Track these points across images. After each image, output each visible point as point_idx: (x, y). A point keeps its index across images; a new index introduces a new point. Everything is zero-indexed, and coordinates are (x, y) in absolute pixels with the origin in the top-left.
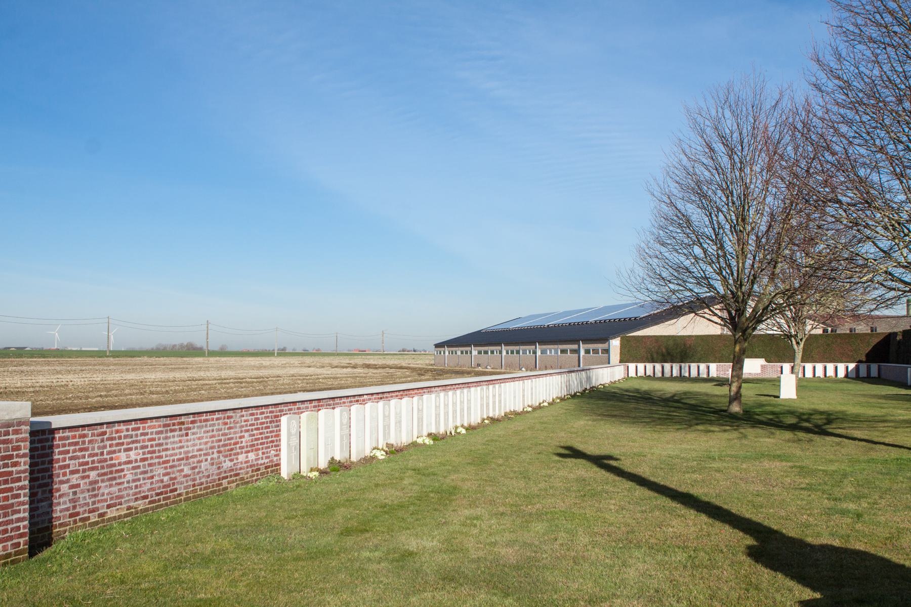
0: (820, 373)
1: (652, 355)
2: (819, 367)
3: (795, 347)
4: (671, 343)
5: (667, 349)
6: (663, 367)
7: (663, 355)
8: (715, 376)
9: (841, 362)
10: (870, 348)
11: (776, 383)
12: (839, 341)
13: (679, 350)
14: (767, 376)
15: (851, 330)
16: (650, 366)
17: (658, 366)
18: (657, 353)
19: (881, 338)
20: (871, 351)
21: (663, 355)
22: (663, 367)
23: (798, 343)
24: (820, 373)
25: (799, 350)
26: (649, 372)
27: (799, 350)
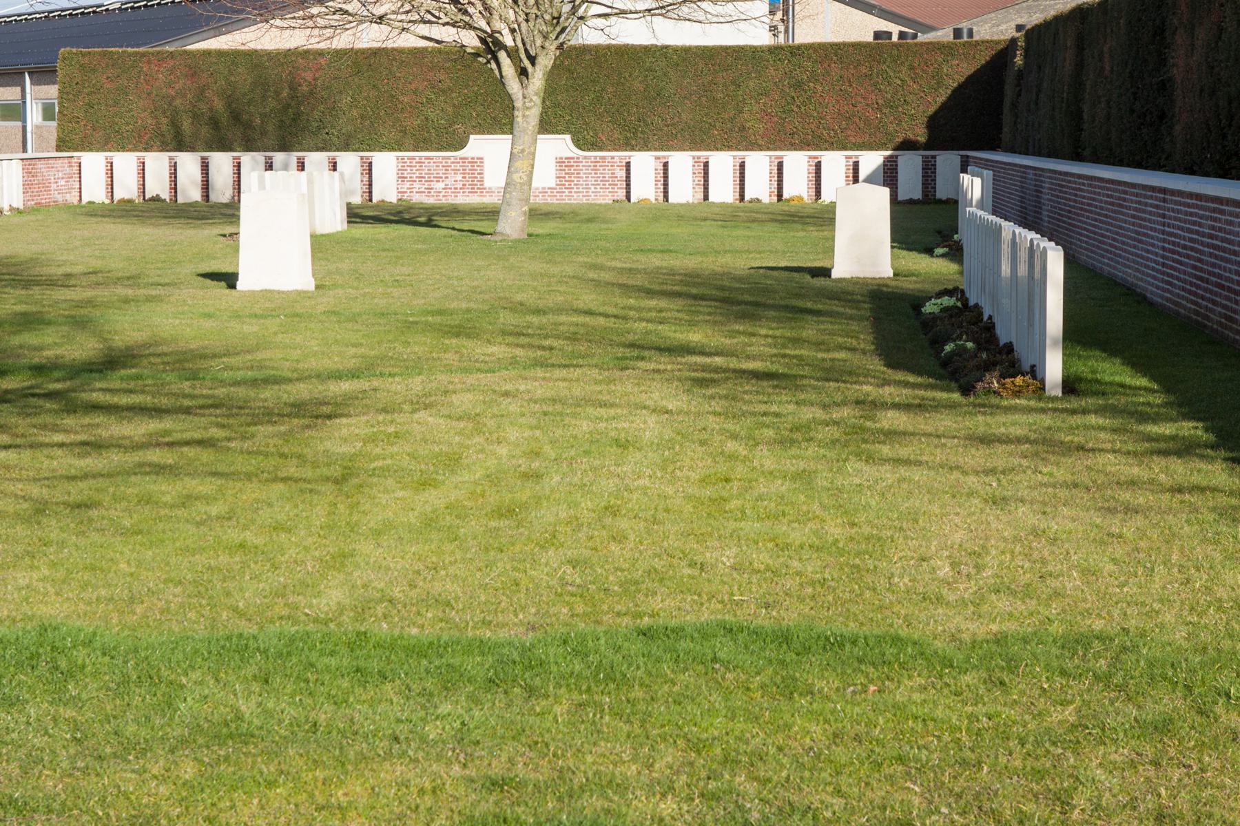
0: (759, 187)
1: (175, 124)
2: (759, 163)
3: (513, 85)
4: (244, 79)
5: (230, 101)
6: (205, 167)
7: (214, 123)
8: (392, 198)
9: (645, 147)
10: (942, 96)
11: (821, 218)
12: (835, 70)
13: (272, 103)
14: (576, 198)
15: (958, 33)
16: (157, 162)
17: (189, 163)
18: (195, 117)
19: (983, 58)
20: (944, 107)
21: (214, 123)
22: (205, 167)
23: (523, 72)
24: (759, 187)
25: (527, 96)
26: (158, 186)
27: (527, 96)
